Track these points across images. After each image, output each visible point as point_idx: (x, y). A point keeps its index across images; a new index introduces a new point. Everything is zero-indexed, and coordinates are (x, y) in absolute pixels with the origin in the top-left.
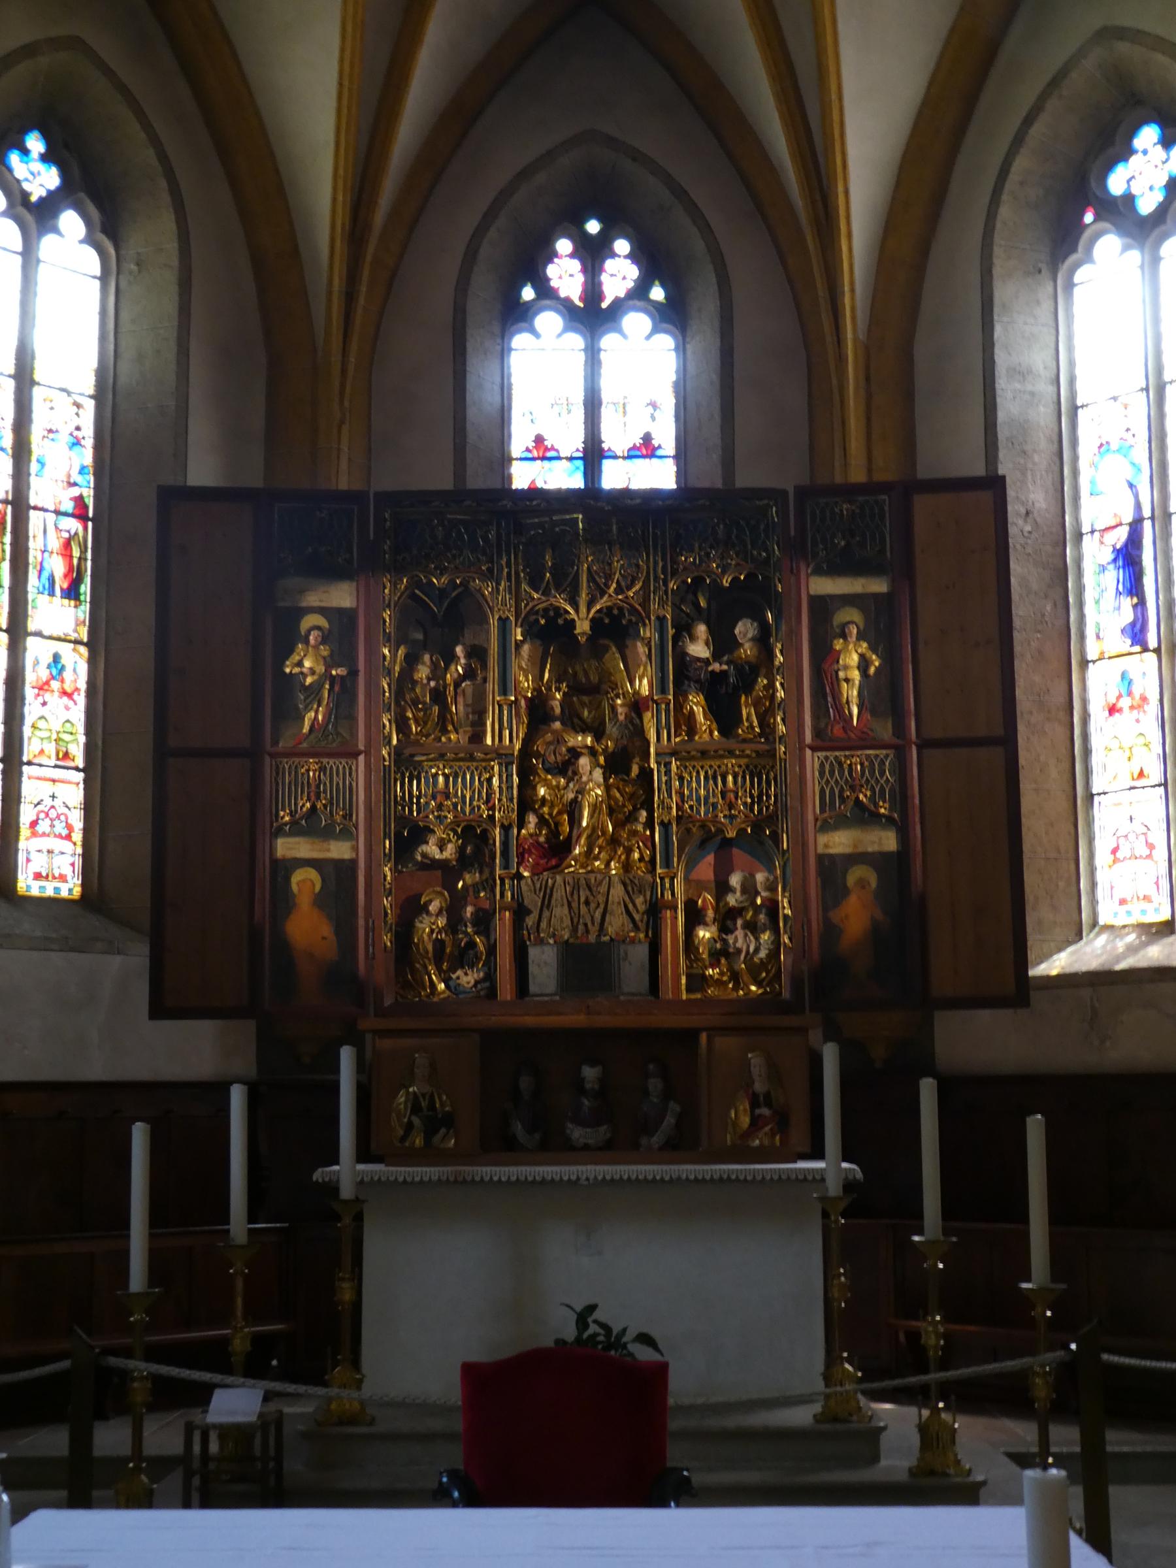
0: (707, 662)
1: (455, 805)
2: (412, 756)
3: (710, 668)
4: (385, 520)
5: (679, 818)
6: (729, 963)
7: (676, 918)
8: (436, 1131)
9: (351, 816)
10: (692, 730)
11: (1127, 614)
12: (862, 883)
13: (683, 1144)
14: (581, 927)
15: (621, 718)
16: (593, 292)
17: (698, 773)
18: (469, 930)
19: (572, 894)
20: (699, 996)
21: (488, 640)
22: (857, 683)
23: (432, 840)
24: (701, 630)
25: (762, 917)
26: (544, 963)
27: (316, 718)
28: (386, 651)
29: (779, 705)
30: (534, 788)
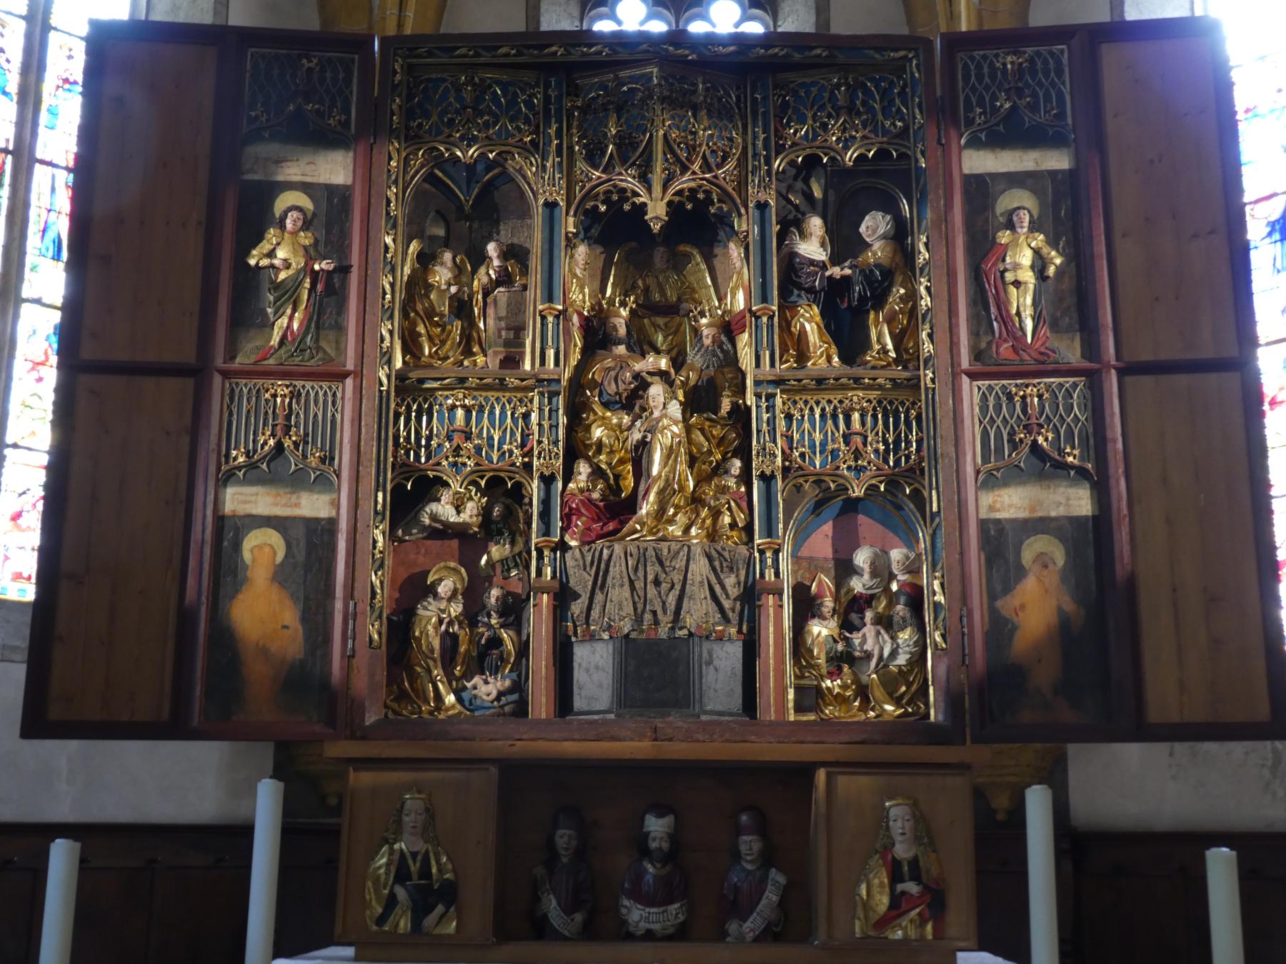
0: (823, 266)
1: (478, 449)
2: (421, 381)
3: (827, 274)
4: (395, 72)
5: (786, 470)
6: (854, 674)
7: (781, 606)
8: (430, 910)
9: (332, 459)
10: (802, 357)
12: (1043, 561)
13: (335, 832)
14: (648, 617)
15: (707, 342)
17: (812, 409)
18: (493, 621)
19: (636, 570)
20: (812, 717)
21: (530, 237)
22: (1031, 287)
23: (446, 496)
24: (815, 224)
25: (900, 609)
26: (595, 666)
27: (289, 326)
28: (389, 240)
29: (924, 316)
30: (588, 429)
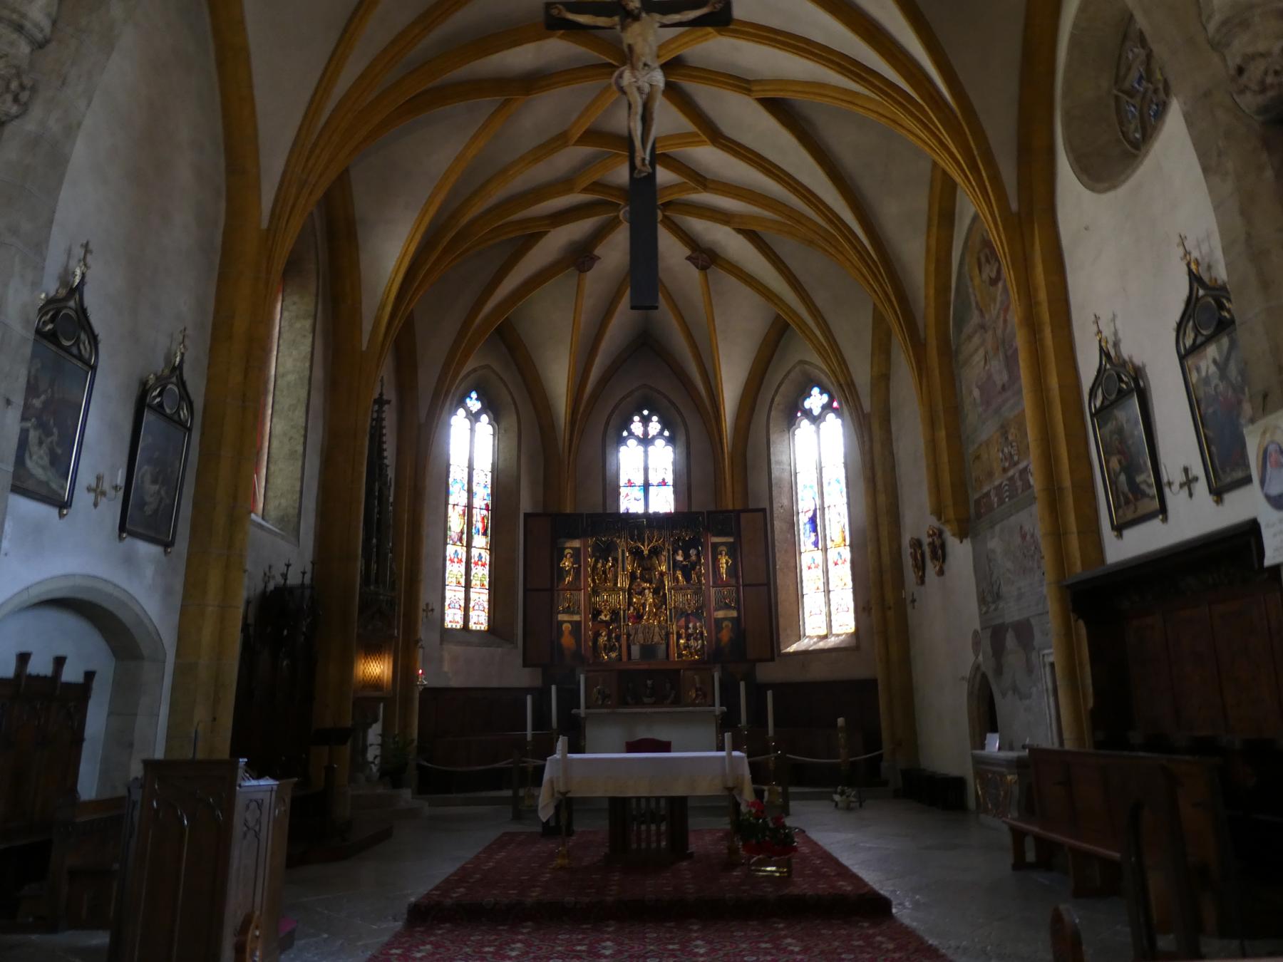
11: (813, 538)
13: (677, 702)
16: (646, 433)
26: (635, 650)
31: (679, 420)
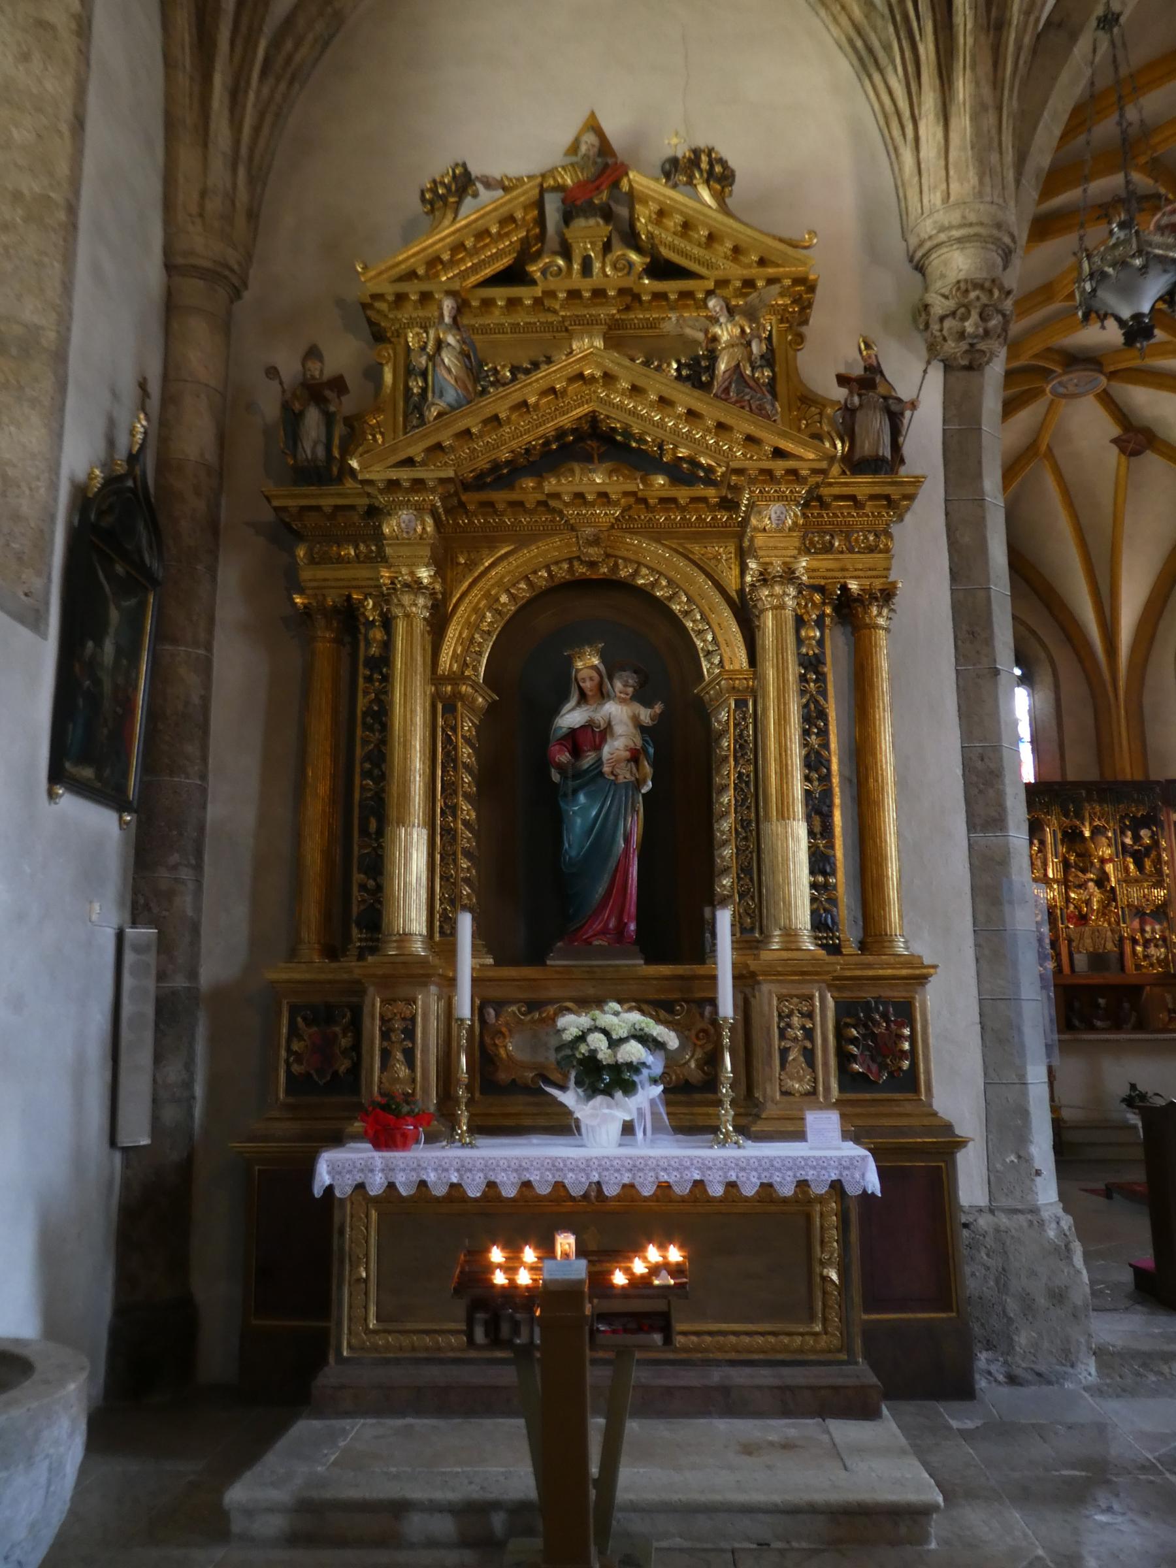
13: (1140, 1027)
25: (1160, 943)
26: (1081, 961)
31: (1043, 655)
